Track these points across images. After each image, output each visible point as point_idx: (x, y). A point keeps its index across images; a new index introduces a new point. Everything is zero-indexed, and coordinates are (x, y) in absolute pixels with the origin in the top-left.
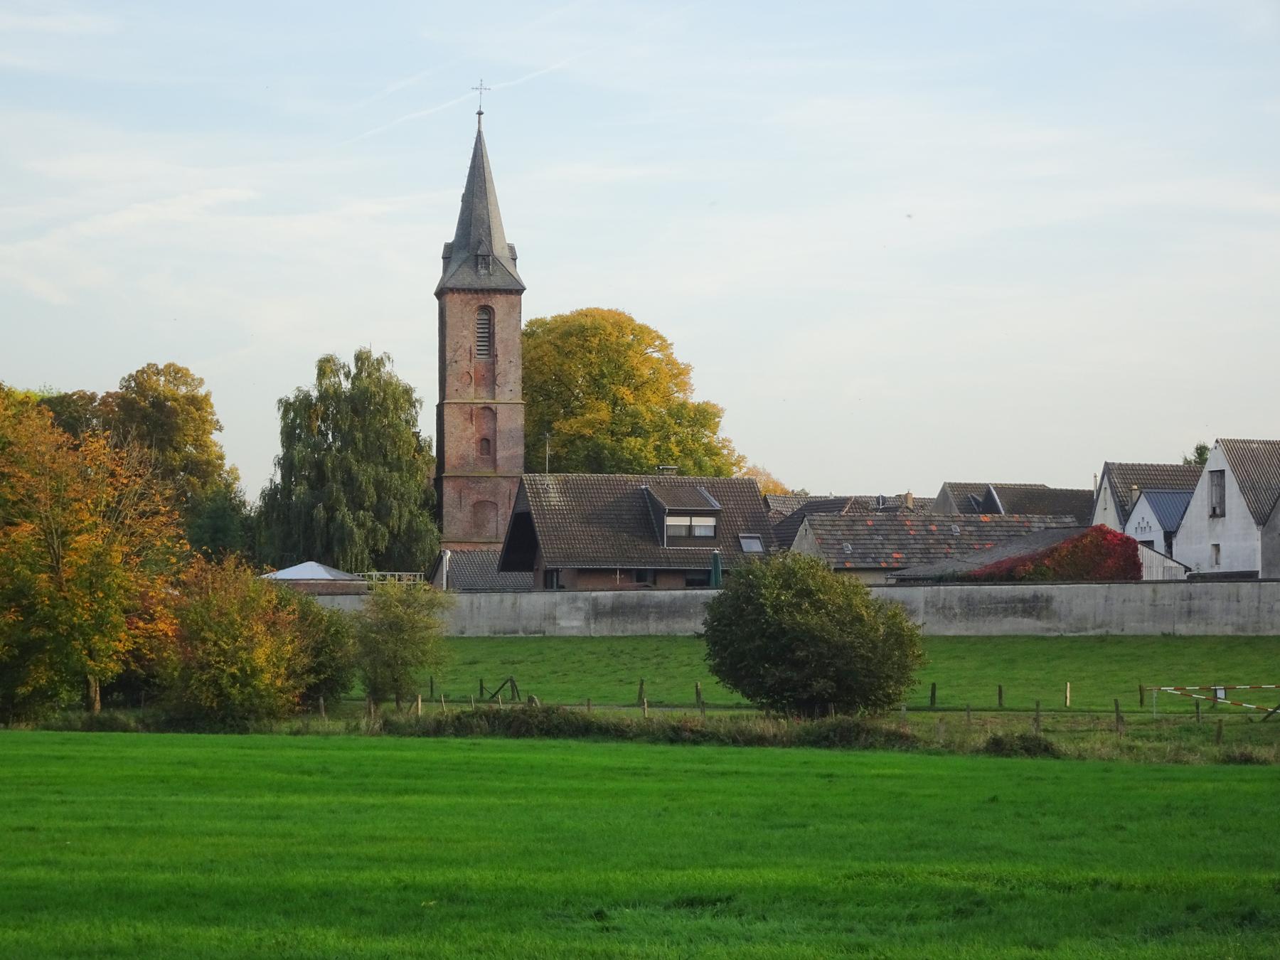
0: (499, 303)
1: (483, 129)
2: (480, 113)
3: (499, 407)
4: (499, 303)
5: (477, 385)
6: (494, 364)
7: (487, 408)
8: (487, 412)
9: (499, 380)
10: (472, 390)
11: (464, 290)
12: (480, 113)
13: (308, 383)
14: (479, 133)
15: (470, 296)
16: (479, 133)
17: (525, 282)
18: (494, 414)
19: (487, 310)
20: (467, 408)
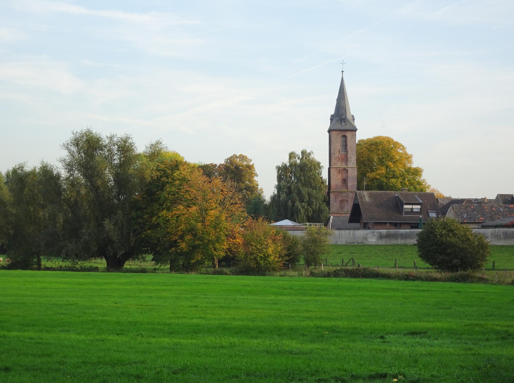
0: (349, 134)
2: (343, 72)
4: (349, 134)
6: (347, 154)
7: (345, 169)
8: (345, 170)
9: (349, 160)
10: (340, 163)
11: (337, 130)
12: (343, 72)
13: (286, 160)
14: (342, 78)
15: (339, 132)
16: (342, 78)
19: (345, 137)
20: (338, 169)
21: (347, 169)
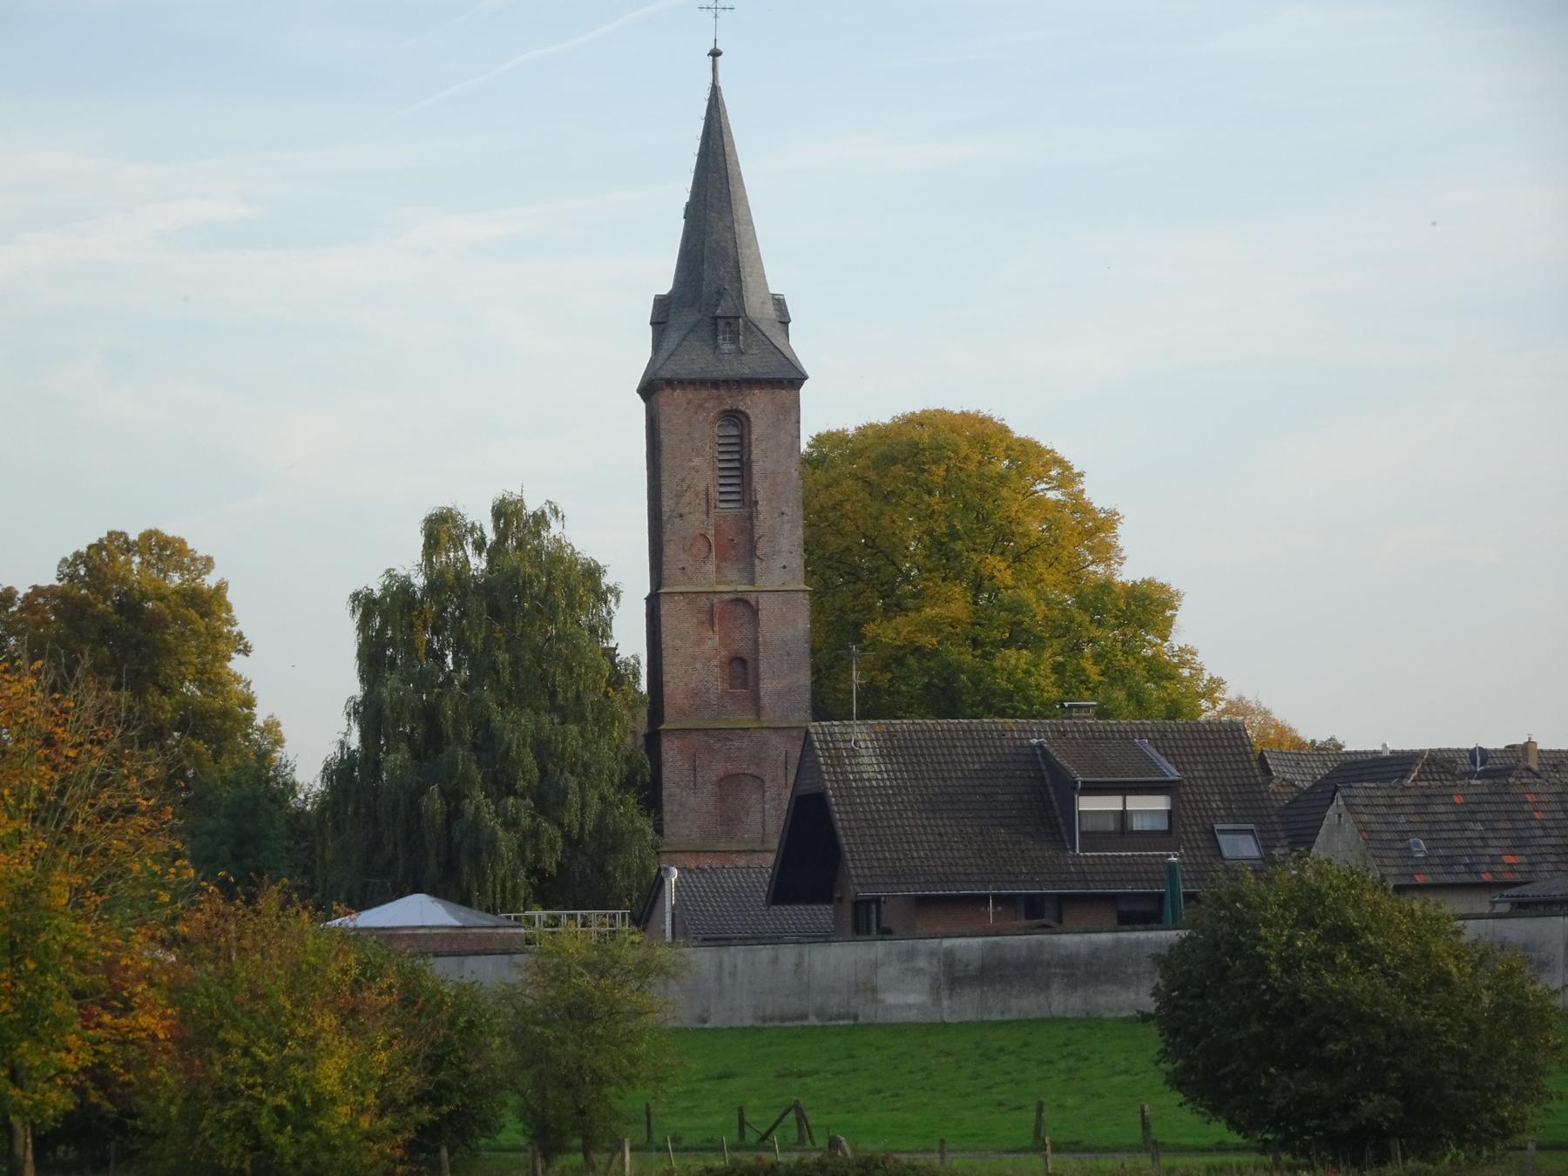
0: (758, 405)
1: (721, 83)
2: (715, 54)
3: (763, 598)
4: (758, 405)
5: (722, 558)
7: (740, 601)
8: (740, 609)
9: (763, 548)
10: (711, 567)
11: (692, 382)
12: (715, 54)
14: (715, 92)
15: (704, 393)
16: (715, 92)
17: (808, 372)
18: (754, 612)
19: (736, 418)
20: (703, 602)
21: (752, 598)
